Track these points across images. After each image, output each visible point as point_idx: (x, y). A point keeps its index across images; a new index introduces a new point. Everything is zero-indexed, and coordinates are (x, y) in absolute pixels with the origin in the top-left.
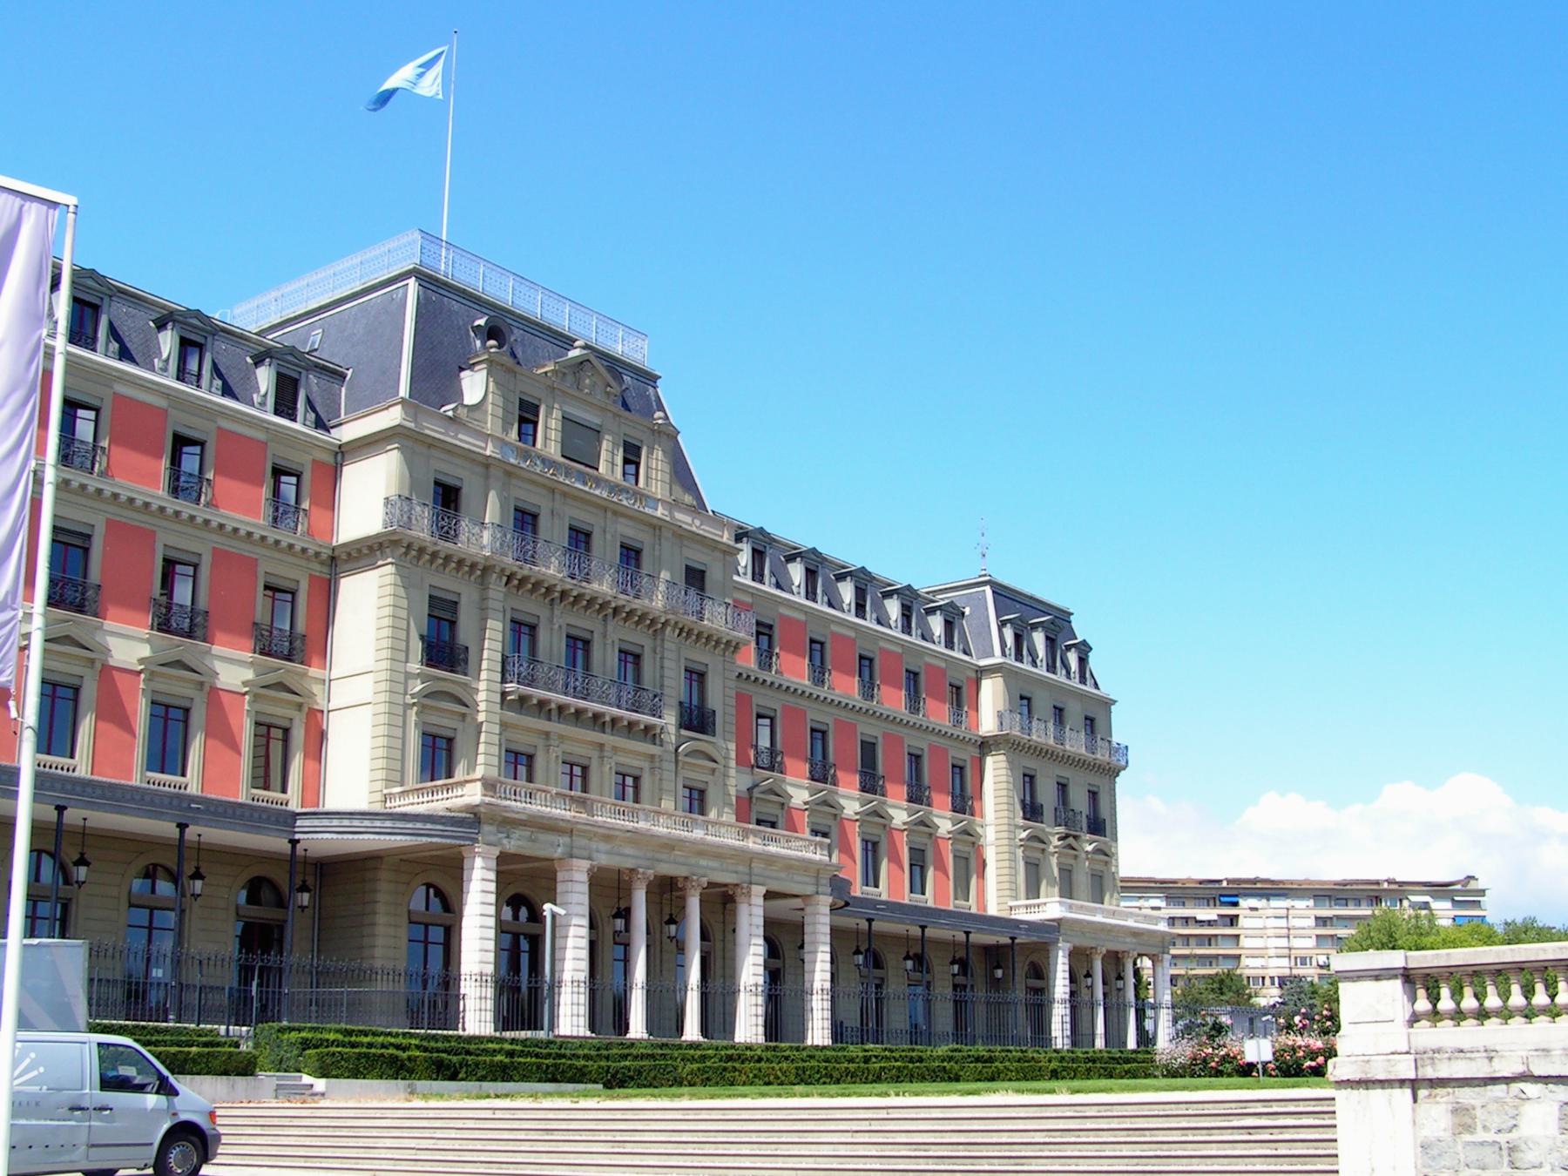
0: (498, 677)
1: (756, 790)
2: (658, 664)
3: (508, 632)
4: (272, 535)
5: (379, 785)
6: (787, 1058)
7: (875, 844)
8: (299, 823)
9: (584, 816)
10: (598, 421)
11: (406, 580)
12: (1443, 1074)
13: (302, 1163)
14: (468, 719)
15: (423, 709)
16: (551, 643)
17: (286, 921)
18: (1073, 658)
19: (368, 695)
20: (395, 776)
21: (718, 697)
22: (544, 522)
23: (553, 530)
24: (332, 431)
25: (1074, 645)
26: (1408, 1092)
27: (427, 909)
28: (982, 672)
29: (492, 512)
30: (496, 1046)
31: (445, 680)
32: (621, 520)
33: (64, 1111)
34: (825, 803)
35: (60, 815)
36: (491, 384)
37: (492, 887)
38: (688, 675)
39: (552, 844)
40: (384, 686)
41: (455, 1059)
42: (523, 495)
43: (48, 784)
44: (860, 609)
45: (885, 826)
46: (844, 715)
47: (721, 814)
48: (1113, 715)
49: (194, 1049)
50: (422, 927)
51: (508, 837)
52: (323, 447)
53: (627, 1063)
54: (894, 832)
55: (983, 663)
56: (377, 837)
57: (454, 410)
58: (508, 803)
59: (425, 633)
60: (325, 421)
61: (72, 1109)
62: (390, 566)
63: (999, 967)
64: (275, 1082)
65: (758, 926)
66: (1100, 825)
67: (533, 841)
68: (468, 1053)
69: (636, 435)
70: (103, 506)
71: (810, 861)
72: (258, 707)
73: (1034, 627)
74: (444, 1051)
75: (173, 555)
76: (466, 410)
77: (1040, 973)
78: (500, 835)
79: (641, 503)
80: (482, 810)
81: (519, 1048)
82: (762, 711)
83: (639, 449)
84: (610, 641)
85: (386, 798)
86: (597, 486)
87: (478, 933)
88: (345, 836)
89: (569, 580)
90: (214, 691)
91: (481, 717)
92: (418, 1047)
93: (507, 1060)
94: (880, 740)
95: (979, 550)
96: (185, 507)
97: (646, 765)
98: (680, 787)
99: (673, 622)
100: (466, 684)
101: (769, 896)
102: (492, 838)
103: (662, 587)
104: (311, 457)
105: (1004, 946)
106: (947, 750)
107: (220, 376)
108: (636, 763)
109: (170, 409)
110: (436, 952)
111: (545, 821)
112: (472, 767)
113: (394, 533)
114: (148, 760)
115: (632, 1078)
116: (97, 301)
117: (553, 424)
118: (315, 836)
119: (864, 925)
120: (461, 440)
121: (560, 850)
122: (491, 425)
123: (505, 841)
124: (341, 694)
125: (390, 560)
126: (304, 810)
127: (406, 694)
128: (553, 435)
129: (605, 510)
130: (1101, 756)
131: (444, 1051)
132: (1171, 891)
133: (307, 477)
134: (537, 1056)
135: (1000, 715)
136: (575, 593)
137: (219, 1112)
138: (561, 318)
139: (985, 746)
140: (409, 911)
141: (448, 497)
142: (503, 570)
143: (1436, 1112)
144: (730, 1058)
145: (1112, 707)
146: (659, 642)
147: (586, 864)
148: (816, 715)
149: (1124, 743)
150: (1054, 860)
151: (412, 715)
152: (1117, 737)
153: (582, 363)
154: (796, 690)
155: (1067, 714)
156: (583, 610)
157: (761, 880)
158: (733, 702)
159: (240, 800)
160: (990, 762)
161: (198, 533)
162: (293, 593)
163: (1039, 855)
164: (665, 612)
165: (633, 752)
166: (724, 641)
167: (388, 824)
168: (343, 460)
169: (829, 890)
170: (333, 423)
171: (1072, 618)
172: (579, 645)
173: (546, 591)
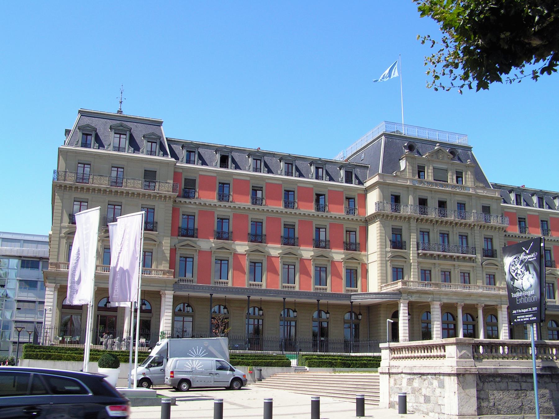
0: (416, 249)
2: (473, 238)
3: (419, 235)
5: (379, 284)
8: (352, 297)
11: (383, 225)
14: (407, 262)
15: (392, 261)
16: (435, 236)
19: (376, 259)
23: (433, 204)
24: (364, 184)
29: (411, 200)
32: (457, 196)
33: (208, 374)
36: (407, 163)
41: (349, 362)
42: (421, 194)
43: (280, 293)
50: (447, 325)
51: (411, 297)
54: (239, 256)
56: (371, 300)
59: (391, 239)
60: (362, 181)
61: (210, 374)
62: (378, 222)
65: (505, 318)
67: (420, 297)
69: (460, 169)
72: (346, 265)
78: (409, 297)
79: (464, 189)
80: (401, 290)
85: (381, 287)
86: (447, 187)
88: (363, 300)
91: (411, 261)
99: (476, 225)
100: (406, 252)
102: (406, 298)
104: (357, 193)
109: (314, 188)
111: (423, 291)
114: (393, 276)
117: (430, 171)
120: (399, 182)
121: (430, 299)
122: (408, 175)
123: (410, 298)
125: (378, 220)
129: (451, 193)
136: (440, 221)
141: (396, 199)
142: (414, 218)
147: (439, 303)
151: (389, 263)
156: (445, 225)
159: (343, 293)
161: (325, 220)
165: (466, 266)
166: (498, 228)
167: (374, 296)
168: (367, 192)
170: (364, 182)
172: (445, 236)
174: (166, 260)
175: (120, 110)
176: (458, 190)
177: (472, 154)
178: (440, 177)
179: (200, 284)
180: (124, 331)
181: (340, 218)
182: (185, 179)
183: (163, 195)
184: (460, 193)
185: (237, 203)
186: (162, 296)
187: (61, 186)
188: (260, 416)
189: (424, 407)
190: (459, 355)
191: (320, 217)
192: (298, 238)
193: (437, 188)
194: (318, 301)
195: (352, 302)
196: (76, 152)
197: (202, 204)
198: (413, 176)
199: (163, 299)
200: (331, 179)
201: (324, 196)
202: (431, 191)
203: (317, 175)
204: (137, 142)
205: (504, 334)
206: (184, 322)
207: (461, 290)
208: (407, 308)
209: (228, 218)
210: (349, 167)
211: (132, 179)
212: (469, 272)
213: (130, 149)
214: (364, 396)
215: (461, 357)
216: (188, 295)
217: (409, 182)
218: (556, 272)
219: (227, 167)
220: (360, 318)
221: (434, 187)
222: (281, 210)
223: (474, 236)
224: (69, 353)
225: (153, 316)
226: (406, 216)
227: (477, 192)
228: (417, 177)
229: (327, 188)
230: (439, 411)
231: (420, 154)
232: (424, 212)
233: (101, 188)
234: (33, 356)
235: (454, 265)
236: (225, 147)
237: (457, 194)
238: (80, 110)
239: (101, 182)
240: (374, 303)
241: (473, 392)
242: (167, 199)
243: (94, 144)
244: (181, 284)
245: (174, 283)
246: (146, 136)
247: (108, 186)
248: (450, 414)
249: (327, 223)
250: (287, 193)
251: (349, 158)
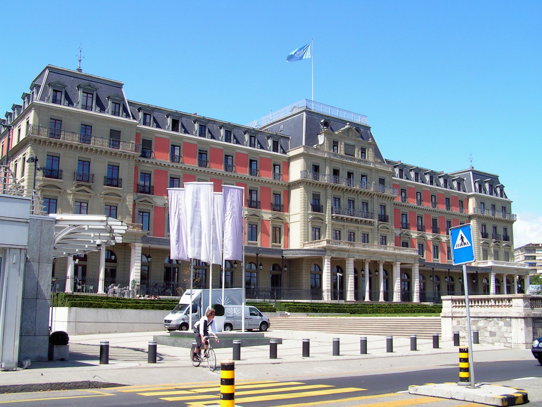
1: (402, 235)
3: (333, 201)
4: (274, 182)
5: (302, 241)
6: (393, 307)
7: (437, 247)
8: (284, 252)
9: (352, 247)
10: (354, 143)
11: (306, 191)
12: (456, 316)
13: (285, 329)
14: (324, 223)
15: (312, 222)
16: (344, 202)
17: (282, 274)
18: (498, 190)
19: (299, 219)
20: (306, 239)
21: (389, 212)
22: (341, 172)
23: (343, 174)
25: (498, 186)
26: (451, 318)
27: (315, 270)
28: (469, 197)
29: (328, 171)
30: (326, 305)
31: (317, 214)
32: (361, 168)
34: (422, 237)
36: (325, 138)
38: (381, 207)
39: (344, 255)
40: (302, 217)
41: (317, 308)
42: (335, 165)
44: (431, 183)
45: (440, 242)
46: (427, 212)
47: (391, 244)
49: (264, 307)
52: (285, 158)
53: (355, 309)
54: (443, 243)
55: (469, 194)
57: (316, 146)
58: (333, 245)
63: (474, 279)
64: (280, 313)
65: (398, 272)
68: (320, 307)
69: (364, 146)
70: (235, 179)
71: (414, 255)
73: (486, 182)
74: (315, 306)
75: (251, 189)
76: (319, 146)
80: (326, 247)
81: (331, 305)
82: (403, 213)
83: (365, 149)
85: (304, 244)
86: (354, 161)
87: (326, 277)
88: (294, 255)
89: (348, 186)
90: (263, 221)
91: (327, 223)
92: (309, 306)
93: (328, 308)
94: (438, 218)
95: (470, 160)
96: (254, 178)
97: (370, 231)
98: (379, 236)
102: (329, 254)
103: (373, 186)
105: (475, 273)
106: (458, 219)
108: (367, 231)
109: (224, 150)
110: (318, 281)
112: (325, 237)
115: (356, 312)
116: (230, 130)
117: (342, 146)
120: (319, 154)
121: (346, 256)
122: (326, 149)
123: (332, 255)
125: (302, 186)
127: (308, 218)
128: (342, 149)
129: (357, 166)
131: (315, 306)
133: (281, 166)
134: (335, 307)
135: (474, 209)
136: (349, 189)
137: (270, 319)
138: (343, 116)
139: (470, 217)
140: (311, 271)
141: (316, 169)
142: (331, 186)
143: (455, 321)
144: (379, 307)
145: (512, 203)
146: (372, 199)
147: (353, 259)
148: (418, 213)
150: (492, 249)
152: (513, 212)
154: (412, 207)
155: (496, 206)
157: (399, 260)
159: (270, 248)
162: (280, 195)
163: (487, 248)
164: (373, 192)
165: (366, 229)
167: (304, 252)
169: (418, 262)
170: (287, 151)
171: (499, 178)
172: (351, 202)
174: (129, 215)
175: (79, 68)
176: (362, 164)
177: (371, 133)
178: (349, 153)
179: (159, 237)
180: (100, 279)
181: (193, 169)
182: (143, 139)
183: (128, 154)
184: (364, 167)
185: (186, 164)
186: (132, 247)
187: (35, 140)
188: (384, 348)
189: (490, 339)
190: (524, 305)
192: (283, 205)
193: (346, 161)
194: (257, 254)
195: (283, 257)
196: (48, 108)
197: (158, 164)
198: (330, 150)
199: (133, 251)
200: (158, 126)
201: (256, 162)
202: (343, 163)
203: (145, 121)
204: (102, 102)
205: (397, 286)
206: (250, 276)
207: (368, 249)
208: (329, 263)
209: (179, 177)
210: (275, 138)
211: (101, 137)
212: (319, 227)
213: (97, 109)
214: (438, 334)
215: (525, 307)
217: (326, 154)
218: (425, 235)
219: (177, 130)
221: (345, 160)
222: (223, 173)
223: (373, 203)
224: (104, 302)
225: (118, 266)
226: (324, 184)
227: (375, 167)
228: (332, 151)
229: (182, 140)
230: (506, 342)
231: (333, 131)
232: (336, 182)
233: (72, 144)
234: (77, 304)
235: (358, 227)
236: (176, 112)
237: (362, 167)
238: (49, 66)
239: (74, 139)
241: (531, 329)
242: (131, 158)
243: (64, 101)
244: (148, 238)
245: (143, 236)
246: (111, 97)
247: (79, 143)
248: (517, 343)
249: (257, 186)
250: (173, 147)
251: (264, 127)
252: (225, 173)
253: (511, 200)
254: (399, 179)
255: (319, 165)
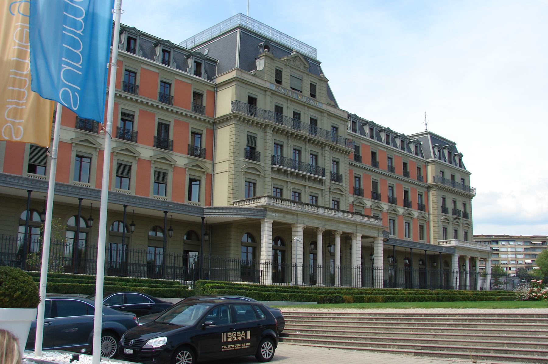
3: (273, 148)
8: (205, 211)
18: (457, 159)
19: (227, 168)
35: (80, 201)
37: (271, 233)
38: (333, 162)
48: (470, 178)
66: (467, 215)
73: (444, 148)
77: (448, 264)
84: (307, 151)
101: (363, 237)
107: (176, 62)
113: (235, 113)
118: (210, 216)
119: (392, 248)
124: (219, 168)
125: (233, 122)
126: (206, 207)
129: (305, 106)
130: (467, 193)
132: (476, 239)
135: (434, 178)
136: (296, 134)
142: (272, 126)
147: (302, 226)
149: (474, 187)
153: (296, 57)
158: (348, 172)
160: (431, 194)
170: (213, 77)
173: (286, 134)
191: (193, 119)
192: (205, 149)
206: (246, 251)
216: (90, 205)
220: (133, 230)
240: (227, 221)
252: (123, 94)
253: (470, 172)
254: (351, 132)
255: (255, 97)
